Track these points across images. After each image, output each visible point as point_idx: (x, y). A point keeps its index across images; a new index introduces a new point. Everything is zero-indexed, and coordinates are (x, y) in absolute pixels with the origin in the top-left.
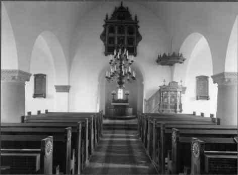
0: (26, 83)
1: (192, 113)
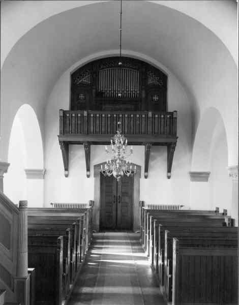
0: (5, 175)
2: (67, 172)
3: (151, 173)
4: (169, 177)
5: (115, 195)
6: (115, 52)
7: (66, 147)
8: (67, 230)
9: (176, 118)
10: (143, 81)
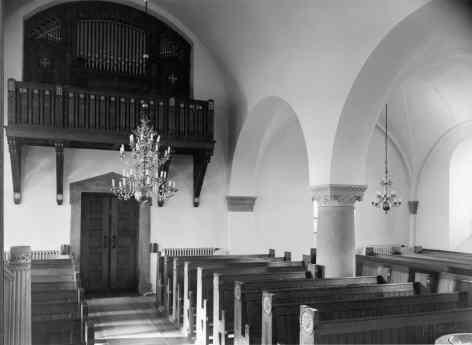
2: (17, 196)
4: (196, 205)
5: (107, 235)
7: (20, 149)
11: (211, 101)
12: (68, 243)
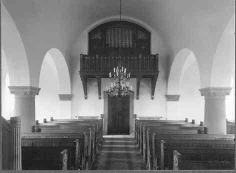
0: (36, 96)
1: (185, 119)
3: (140, 96)
4: (153, 99)
6: (116, 17)
8: (75, 141)
9: (158, 59)
10: (135, 37)
11: (158, 54)
12: (103, 113)
